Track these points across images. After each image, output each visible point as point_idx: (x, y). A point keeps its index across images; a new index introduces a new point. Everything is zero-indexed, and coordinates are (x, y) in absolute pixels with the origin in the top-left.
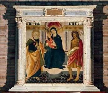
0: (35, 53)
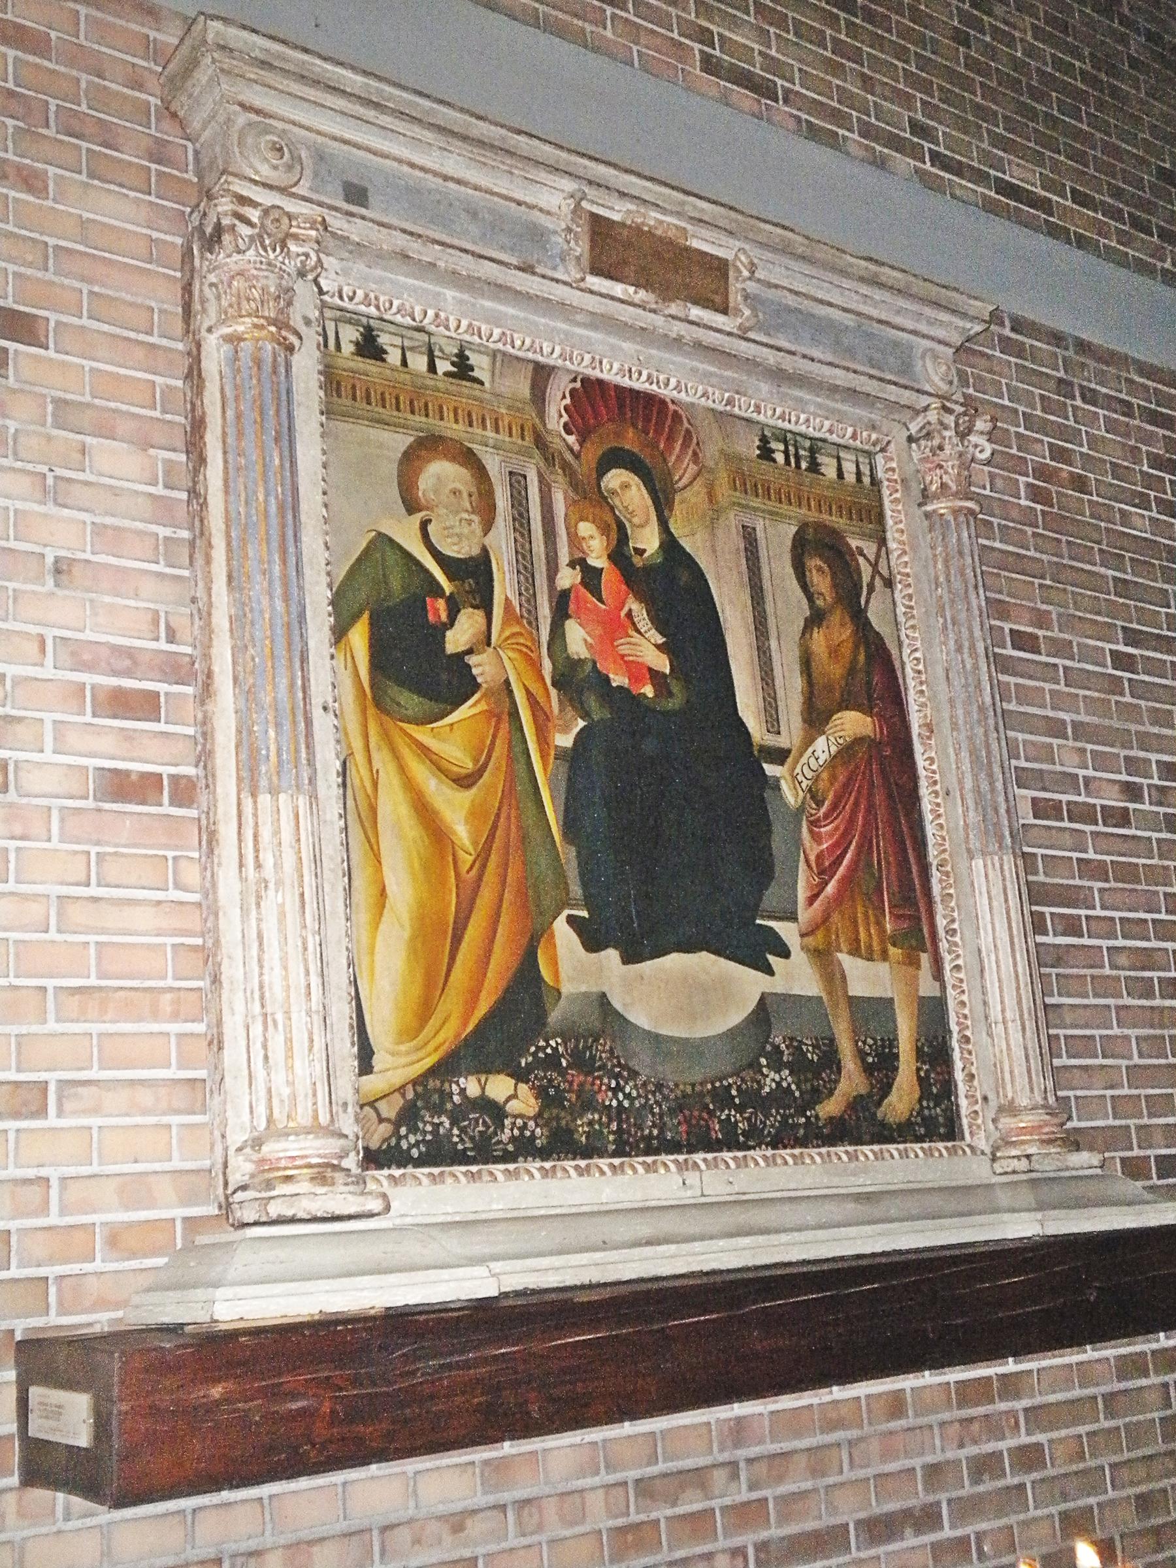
0: (456, 734)
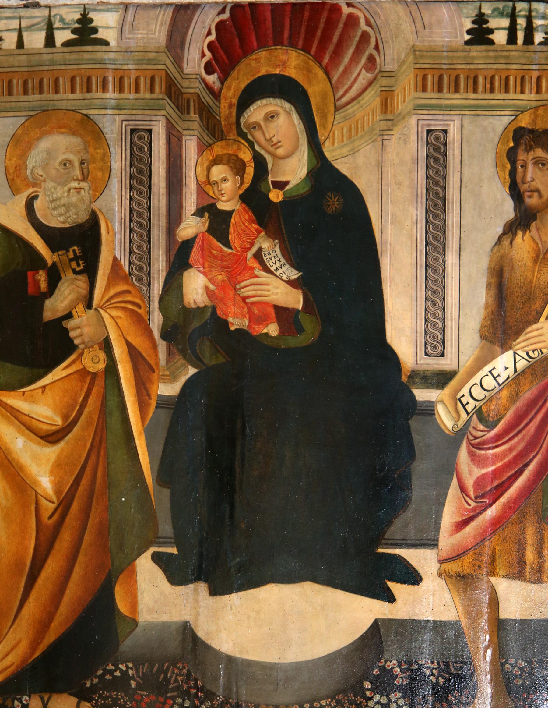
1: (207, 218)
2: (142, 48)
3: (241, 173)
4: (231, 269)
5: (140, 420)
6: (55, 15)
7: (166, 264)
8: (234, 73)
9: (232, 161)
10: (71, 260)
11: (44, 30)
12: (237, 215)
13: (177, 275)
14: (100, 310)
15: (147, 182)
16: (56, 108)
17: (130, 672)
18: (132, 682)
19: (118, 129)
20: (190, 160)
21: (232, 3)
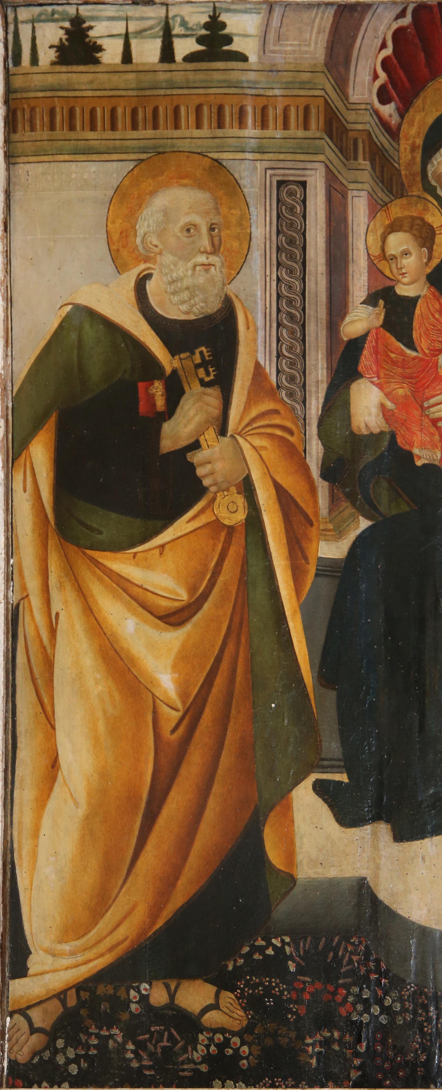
0: (160, 566)
1: (382, 307)
2: (292, 66)
3: (428, 244)
4: (417, 380)
5: (293, 593)
6: (175, 16)
7: (327, 372)
8: (419, 102)
9: (417, 227)
10: (197, 366)
11: (159, 37)
12: (424, 302)
13: (341, 387)
14: (238, 438)
15: (301, 256)
16: (175, 149)
17: (287, 949)
18: (290, 963)
19: (260, 180)
20: (359, 225)
21: (416, 2)
